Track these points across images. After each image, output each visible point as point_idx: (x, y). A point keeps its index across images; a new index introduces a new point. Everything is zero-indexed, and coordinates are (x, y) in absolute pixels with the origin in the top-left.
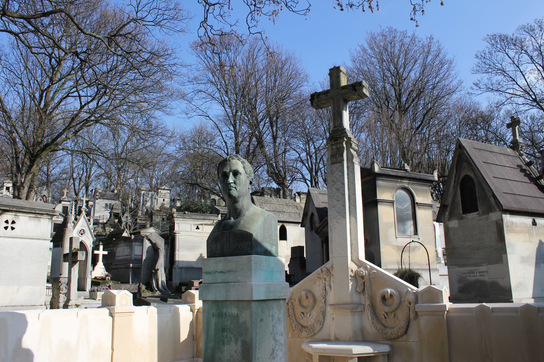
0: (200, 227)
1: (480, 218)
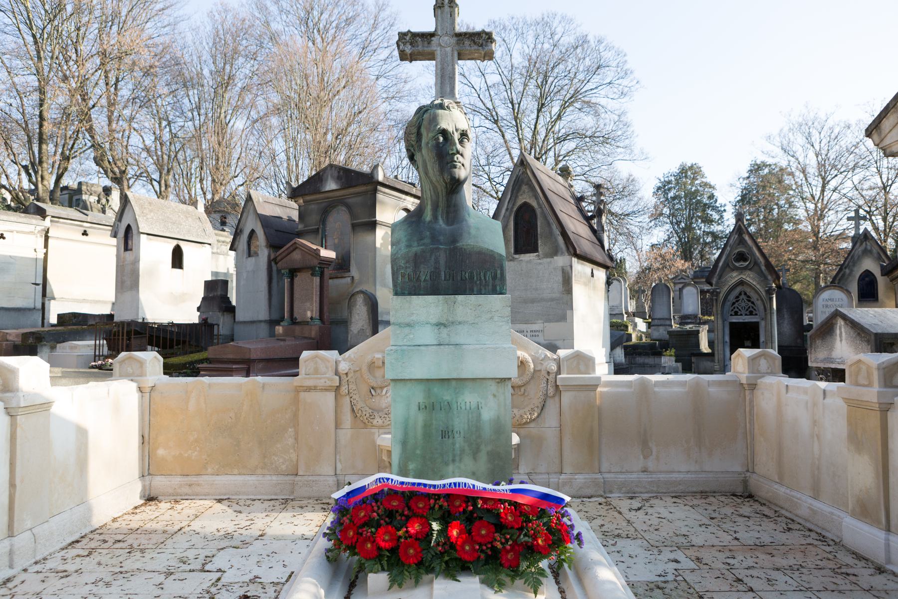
0: (89, 231)
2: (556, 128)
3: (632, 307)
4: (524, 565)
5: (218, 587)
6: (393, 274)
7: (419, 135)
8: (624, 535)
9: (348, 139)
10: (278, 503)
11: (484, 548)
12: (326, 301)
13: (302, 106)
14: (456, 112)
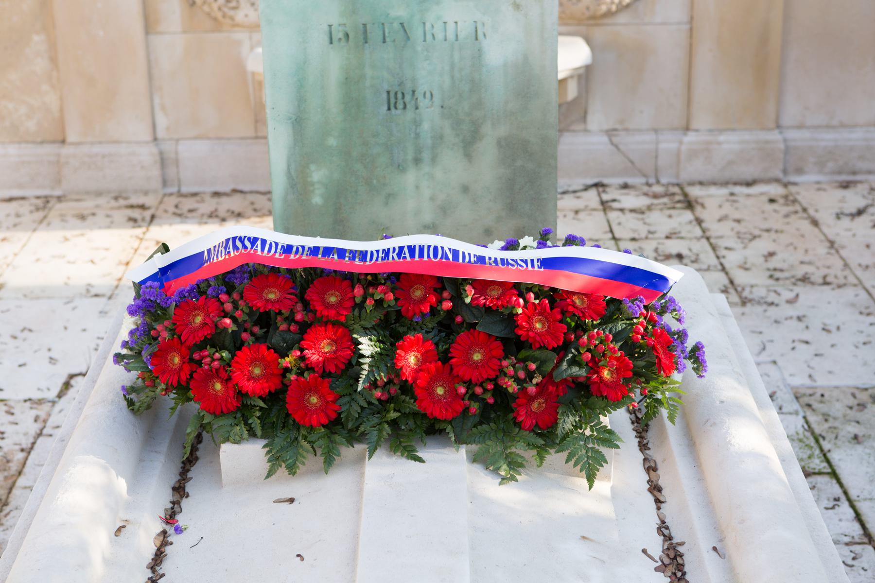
4: (567, 422)
8: (817, 277)
10: (24, 208)
11: (479, 390)
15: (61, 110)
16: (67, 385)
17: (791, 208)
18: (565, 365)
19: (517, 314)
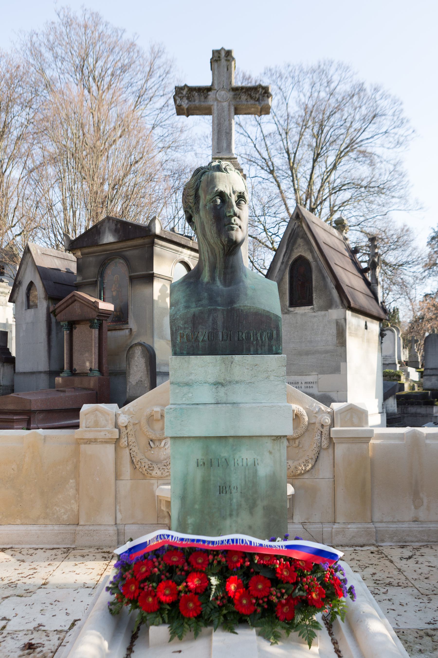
1: (314, 314)
2: (332, 178)
3: (405, 356)
4: (299, 618)
5: (4, 635)
6: (172, 334)
7: (197, 197)
8: (395, 583)
9: (125, 189)
10: (59, 552)
11: (261, 601)
12: (105, 354)
13: (78, 156)
14: (234, 174)
15: (78, 511)
16: (73, 625)
17: (381, 556)
18: (297, 591)
19: (276, 568)
